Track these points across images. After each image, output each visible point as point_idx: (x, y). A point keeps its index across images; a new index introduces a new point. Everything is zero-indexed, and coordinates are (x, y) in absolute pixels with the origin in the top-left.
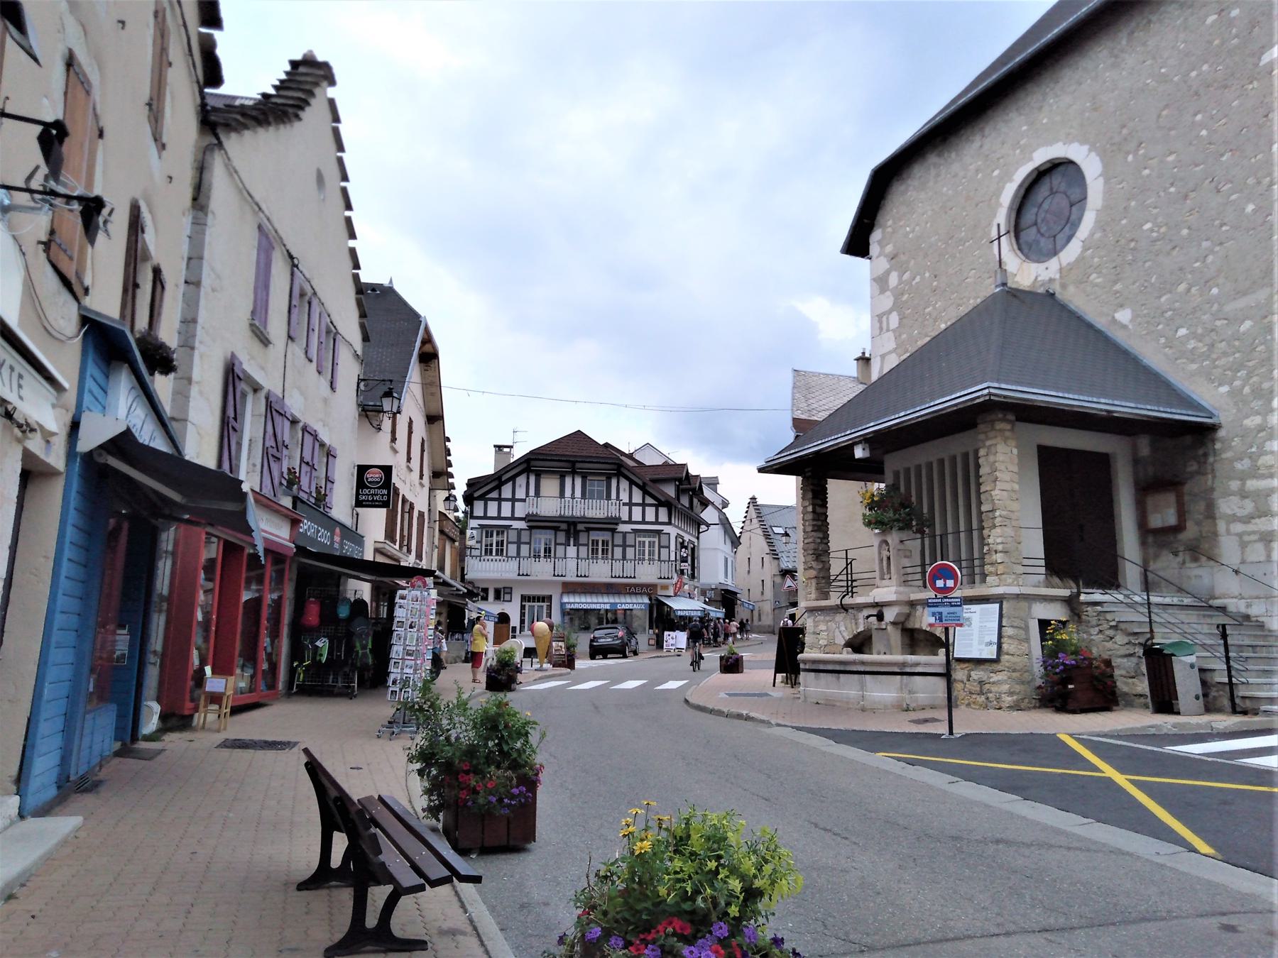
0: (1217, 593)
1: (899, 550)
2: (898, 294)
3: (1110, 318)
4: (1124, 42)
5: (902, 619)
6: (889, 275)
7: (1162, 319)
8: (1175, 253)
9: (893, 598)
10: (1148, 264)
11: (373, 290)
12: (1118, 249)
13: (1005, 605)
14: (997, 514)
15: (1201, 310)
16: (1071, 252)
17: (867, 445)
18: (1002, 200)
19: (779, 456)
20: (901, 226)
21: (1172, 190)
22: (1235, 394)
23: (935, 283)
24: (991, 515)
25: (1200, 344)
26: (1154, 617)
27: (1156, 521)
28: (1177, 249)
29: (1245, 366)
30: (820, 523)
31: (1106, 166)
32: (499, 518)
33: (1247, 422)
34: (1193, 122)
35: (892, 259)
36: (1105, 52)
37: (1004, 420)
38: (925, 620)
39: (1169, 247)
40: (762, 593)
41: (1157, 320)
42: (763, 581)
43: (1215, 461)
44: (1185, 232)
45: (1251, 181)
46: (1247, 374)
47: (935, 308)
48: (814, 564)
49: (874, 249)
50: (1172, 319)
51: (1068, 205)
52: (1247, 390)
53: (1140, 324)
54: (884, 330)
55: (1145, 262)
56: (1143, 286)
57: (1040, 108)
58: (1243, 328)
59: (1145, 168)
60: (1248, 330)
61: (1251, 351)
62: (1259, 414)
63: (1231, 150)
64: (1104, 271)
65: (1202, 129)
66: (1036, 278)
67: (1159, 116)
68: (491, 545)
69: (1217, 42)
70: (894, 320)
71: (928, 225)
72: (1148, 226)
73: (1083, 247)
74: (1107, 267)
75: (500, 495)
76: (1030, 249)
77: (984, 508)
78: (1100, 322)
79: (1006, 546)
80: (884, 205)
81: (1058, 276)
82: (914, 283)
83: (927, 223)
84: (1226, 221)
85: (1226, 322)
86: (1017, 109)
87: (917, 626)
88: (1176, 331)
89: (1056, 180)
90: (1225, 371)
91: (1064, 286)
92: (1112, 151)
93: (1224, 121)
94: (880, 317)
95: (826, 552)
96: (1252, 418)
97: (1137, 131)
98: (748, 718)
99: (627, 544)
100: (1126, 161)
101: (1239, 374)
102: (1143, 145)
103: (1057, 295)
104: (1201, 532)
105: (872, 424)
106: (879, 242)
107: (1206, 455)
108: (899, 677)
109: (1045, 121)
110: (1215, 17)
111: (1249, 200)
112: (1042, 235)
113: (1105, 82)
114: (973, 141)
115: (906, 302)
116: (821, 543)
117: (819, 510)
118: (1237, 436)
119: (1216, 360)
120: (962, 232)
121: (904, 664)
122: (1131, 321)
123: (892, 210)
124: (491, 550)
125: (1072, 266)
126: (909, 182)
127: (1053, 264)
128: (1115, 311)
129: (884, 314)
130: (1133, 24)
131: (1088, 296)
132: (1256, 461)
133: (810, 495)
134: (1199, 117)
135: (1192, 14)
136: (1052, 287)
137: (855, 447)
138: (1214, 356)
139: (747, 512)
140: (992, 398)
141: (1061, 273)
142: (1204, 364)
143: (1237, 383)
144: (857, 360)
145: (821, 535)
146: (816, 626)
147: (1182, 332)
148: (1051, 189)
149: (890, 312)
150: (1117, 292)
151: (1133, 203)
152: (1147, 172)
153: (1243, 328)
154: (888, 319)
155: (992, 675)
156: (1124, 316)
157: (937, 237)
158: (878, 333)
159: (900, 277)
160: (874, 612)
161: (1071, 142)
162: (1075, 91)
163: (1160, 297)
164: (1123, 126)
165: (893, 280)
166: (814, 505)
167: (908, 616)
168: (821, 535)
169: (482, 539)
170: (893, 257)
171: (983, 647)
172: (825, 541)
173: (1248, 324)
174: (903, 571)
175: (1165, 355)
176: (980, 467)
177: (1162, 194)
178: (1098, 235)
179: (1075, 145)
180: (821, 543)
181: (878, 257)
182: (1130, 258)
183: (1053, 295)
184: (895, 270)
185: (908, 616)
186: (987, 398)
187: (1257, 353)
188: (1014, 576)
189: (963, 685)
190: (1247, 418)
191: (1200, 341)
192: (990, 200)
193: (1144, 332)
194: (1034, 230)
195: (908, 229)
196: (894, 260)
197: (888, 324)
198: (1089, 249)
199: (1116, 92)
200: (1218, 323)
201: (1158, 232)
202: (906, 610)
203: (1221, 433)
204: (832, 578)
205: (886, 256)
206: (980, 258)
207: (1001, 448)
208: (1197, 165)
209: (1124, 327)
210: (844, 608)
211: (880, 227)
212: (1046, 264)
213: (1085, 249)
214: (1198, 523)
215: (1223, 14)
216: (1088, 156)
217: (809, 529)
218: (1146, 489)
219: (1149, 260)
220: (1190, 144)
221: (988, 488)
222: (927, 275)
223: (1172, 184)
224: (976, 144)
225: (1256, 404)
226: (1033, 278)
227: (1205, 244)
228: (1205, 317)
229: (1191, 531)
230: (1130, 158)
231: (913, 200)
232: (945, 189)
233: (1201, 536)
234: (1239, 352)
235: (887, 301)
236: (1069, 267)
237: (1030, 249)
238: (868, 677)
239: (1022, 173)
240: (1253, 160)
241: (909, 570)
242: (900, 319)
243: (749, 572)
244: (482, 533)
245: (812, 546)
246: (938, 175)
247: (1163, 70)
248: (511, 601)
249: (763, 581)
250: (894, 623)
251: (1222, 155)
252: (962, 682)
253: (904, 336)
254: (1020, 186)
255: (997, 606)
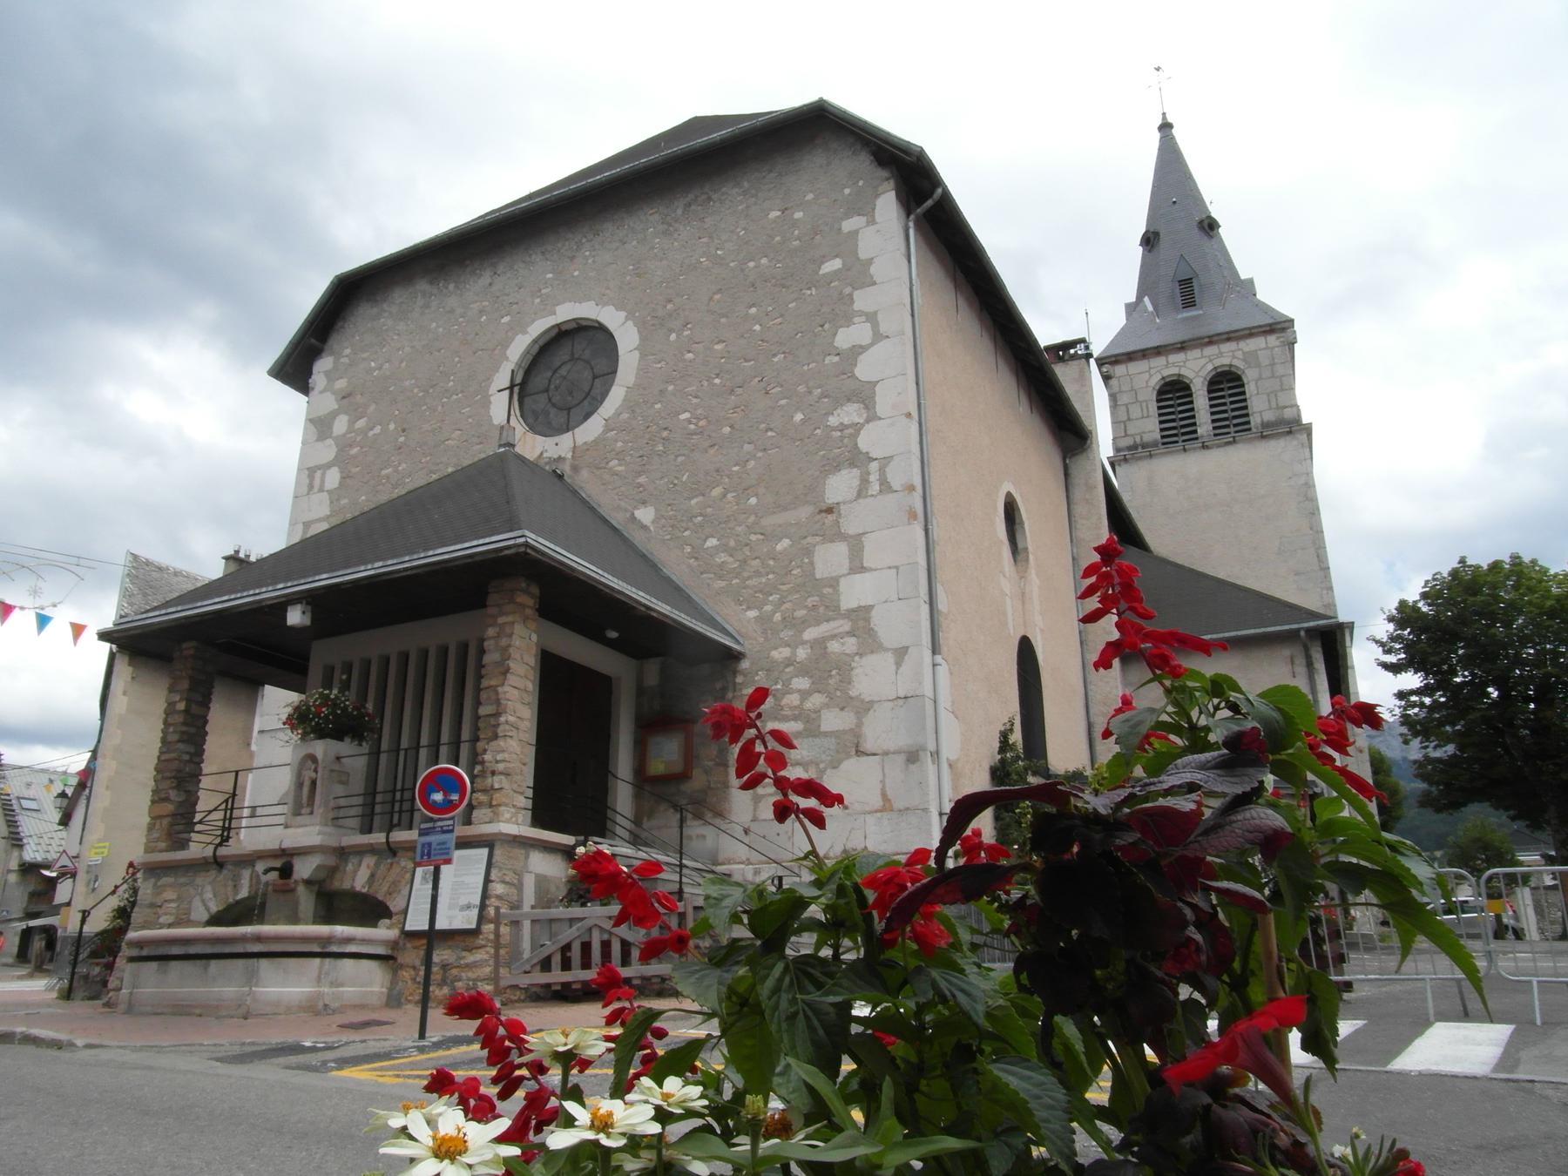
0: (721, 858)
1: (332, 771)
2: (344, 445)
3: (628, 515)
4: (679, 212)
5: (322, 875)
7: (690, 524)
8: (712, 451)
9: (315, 840)
10: (680, 459)
12: (647, 436)
13: (498, 852)
14: (502, 719)
15: (735, 520)
16: (591, 430)
17: (309, 608)
18: (559, 309)
19: (144, 616)
20: (364, 359)
21: (717, 381)
22: (763, 620)
23: (402, 439)
24: (493, 721)
25: (731, 559)
26: (684, 880)
27: (657, 767)
28: (716, 447)
29: (779, 590)
30: (193, 730)
31: (644, 339)
33: (775, 654)
34: (747, 314)
35: (344, 398)
36: (657, 217)
37: (526, 592)
38: (359, 877)
39: (707, 444)
41: (684, 525)
43: (734, 697)
44: (727, 430)
45: (802, 389)
46: (779, 599)
47: (396, 471)
48: (173, 794)
49: (318, 378)
50: (701, 525)
51: (590, 377)
52: (778, 617)
53: (664, 527)
54: (316, 490)
55: (677, 456)
56: (672, 483)
57: (572, 258)
58: (779, 547)
59: (689, 352)
60: (785, 549)
61: (786, 574)
62: (789, 646)
63: (784, 353)
64: (628, 459)
66: (542, 454)
67: (711, 299)
69: (778, 238)
70: (333, 478)
71: (404, 364)
72: (686, 415)
73: (606, 426)
74: (631, 455)
76: (536, 419)
77: (483, 711)
78: (617, 519)
79: (508, 765)
80: (343, 327)
81: (569, 456)
82: (371, 433)
83: (402, 362)
84: (772, 426)
85: (761, 537)
86: (543, 253)
87: (346, 885)
88: (705, 541)
89: (580, 346)
90: (756, 592)
91: (575, 469)
93: (779, 320)
94: (311, 471)
95: (196, 776)
96: (781, 649)
97: (684, 310)
98: (29, 1040)
100: (668, 340)
101: (771, 598)
102: (689, 326)
103: (565, 478)
104: (709, 782)
106: (327, 374)
107: (724, 689)
108: (317, 961)
109: (576, 273)
110: (779, 213)
111: (798, 409)
112: (554, 405)
113: (653, 248)
115: (355, 457)
116: (190, 761)
117: (195, 709)
118: (762, 669)
119: (749, 578)
120: (450, 381)
121: (329, 940)
122: (653, 522)
123: (353, 337)
125: (588, 447)
126: (385, 306)
128: (636, 508)
129: (319, 467)
130: (691, 196)
131: (604, 484)
132: (780, 701)
134: (753, 310)
135: (755, 204)
136: (561, 466)
137: (289, 608)
138: (746, 574)
140: (529, 551)
141: (574, 452)
142: (734, 582)
143: (768, 608)
144: (227, 558)
145: (192, 750)
147: (712, 542)
148: (572, 354)
149: (329, 466)
150: (640, 485)
151: (671, 388)
153: (779, 547)
154: (323, 475)
155: (464, 954)
156: (645, 515)
157: (413, 381)
158: (306, 492)
159: (352, 423)
160: (278, 864)
161: (605, 304)
162: (617, 249)
163: (690, 499)
164: (670, 301)
165: (341, 425)
166: (189, 701)
167: (333, 871)
168: (192, 750)
170: (345, 396)
171: (457, 912)
172: (197, 760)
173: (786, 542)
174: (332, 804)
175: (689, 566)
176: (484, 652)
177: (705, 383)
178: (625, 416)
180: (190, 761)
181: (321, 392)
182: (661, 448)
183: (561, 477)
184: (346, 413)
185: (333, 871)
186: (522, 549)
187: (793, 578)
188: (513, 810)
189: (413, 973)
190: (776, 648)
191: (731, 556)
192: (494, 349)
193: (668, 537)
194: (543, 398)
195: (373, 364)
196: (346, 401)
197: (323, 481)
198: (612, 430)
199: (665, 262)
200: (753, 537)
201: (696, 425)
202: (331, 861)
203: (745, 665)
204: (198, 817)
206: (470, 417)
207: (519, 629)
208: (746, 361)
209: (644, 527)
210: (218, 863)
211: (332, 354)
213: (608, 429)
214: (707, 772)
215: (786, 212)
217: (173, 737)
218: (651, 724)
219: (684, 455)
221: (493, 683)
222: (392, 426)
223: (717, 376)
224: (486, 278)
225: (786, 634)
226: (538, 453)
227: (747, 447)
228: (739, 529)
229: (698, 781)
230: (673, 337)
233: (709, 787)
234: (773, 573)
235: (327, 451)
236: (585, 447)
237: (536, 419)
238: (264, 963)
239: (539, 327)
240: (806, 368)
241: (342, 802)
242: (343, 478)
245: (175, 765)
246: (427, 306)
247: (719, 252)
250: (308, 883)
251: (775, 355)
252: (414, 968)
253: (344, 501)
254: (535, 341)
255: (485, 852)
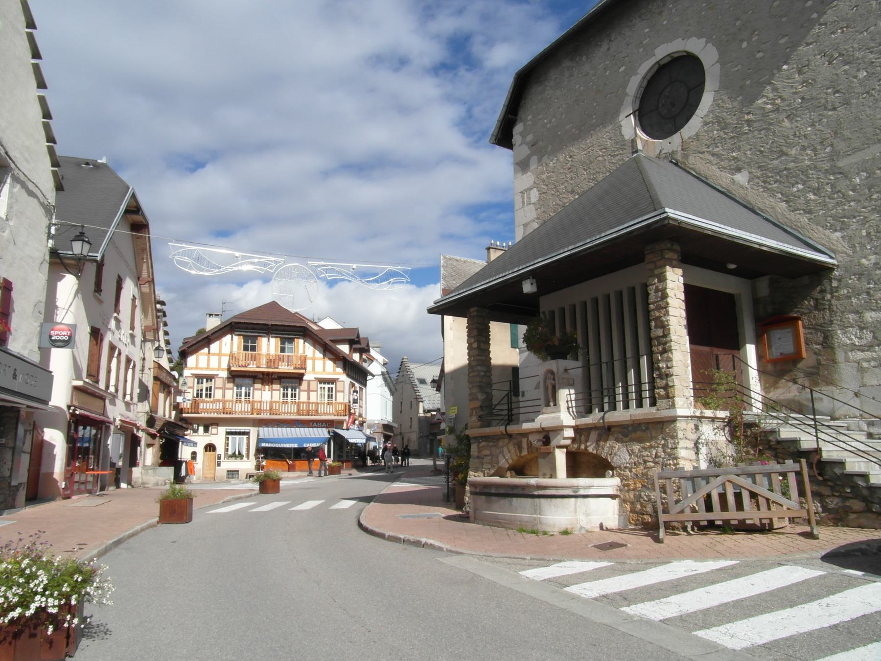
6: (530, 159)
11: (87, 164)
18: (628, 90)
31: (722, 53)
32: (208, 368)
35: (533, 146)
40: (411, 427)
42: (411, 418)
49: (517, 139)
57: (660, 13)
59: (759, 52)
65: (813, 13)
66: (661, 151)
68: (202, 390)
71: (564, 116)
75: (209, 351)
83: (562, 115)
86: (640, 16)
91: (686, 156)
92: (727, 41)
99: (311, 389)
102: (756, 33)
105: (540, 260)
108: (573, 500)
109: (665, 22)
114: (601, 46)
117: (483, 346)
124: (201, 394)
126: (546, 83)
127: (676, 139)
129: (526, 190)
133: (475, 332)
137: (523, 282)
139: (400, 369)
146: (479, 452)
149: (530, 189)
151: (748, 82)
152: (760, 55)
157: (571, 125)
158: (521, 207)
169: (194, 385)
179: (694, 39)
195: (546, 121)
205: (527, 144)
212: (669, 139)
216: (706, 46)
220: (802, 26)
224: (605, 47)
230: (745, 45)
231: (550, 98)
232: (578, 86)
239: (645, 67)
243: (401, 412)
244: (194, 380)
248: (217, 434)
249: (411, 418)
